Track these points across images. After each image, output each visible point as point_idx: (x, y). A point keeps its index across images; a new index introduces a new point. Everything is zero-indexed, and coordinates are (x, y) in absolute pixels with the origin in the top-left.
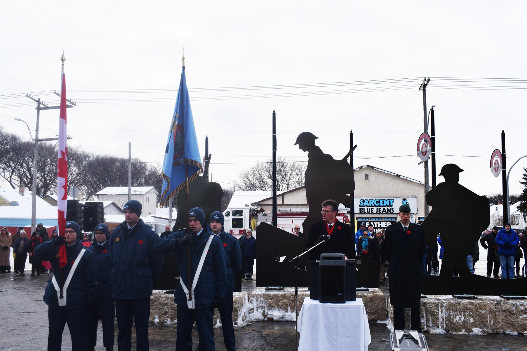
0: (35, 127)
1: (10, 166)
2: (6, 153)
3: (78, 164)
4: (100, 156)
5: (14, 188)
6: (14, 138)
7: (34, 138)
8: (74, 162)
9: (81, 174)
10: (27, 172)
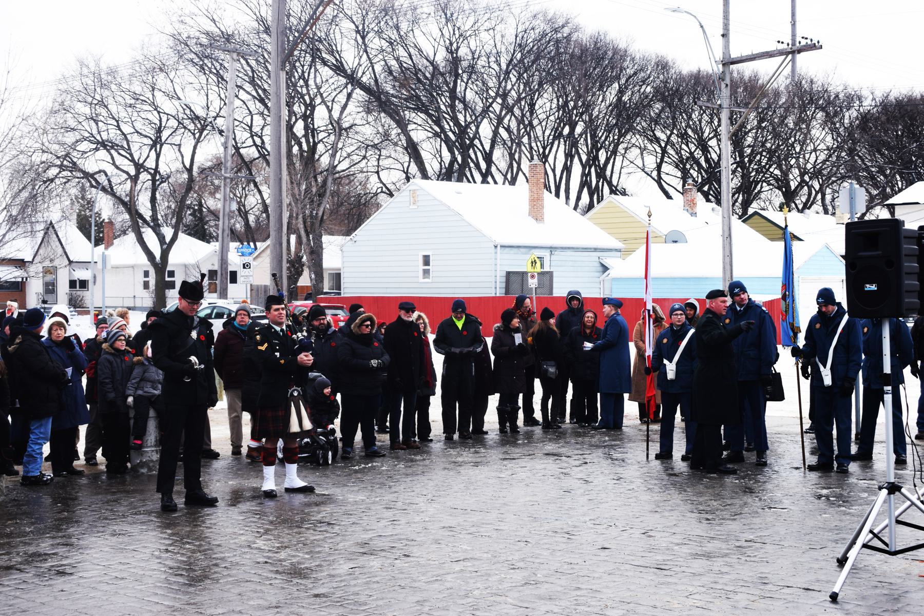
0: (721, 25)
1: (658, 140)
2: (644, 107)
3: (830, 121)
4: (892, 98)
5: (669, 197)
6: (662, 66)
7: (719, 55)
8: (820, 115)
9: (840, 148)
10: (698, 154)
